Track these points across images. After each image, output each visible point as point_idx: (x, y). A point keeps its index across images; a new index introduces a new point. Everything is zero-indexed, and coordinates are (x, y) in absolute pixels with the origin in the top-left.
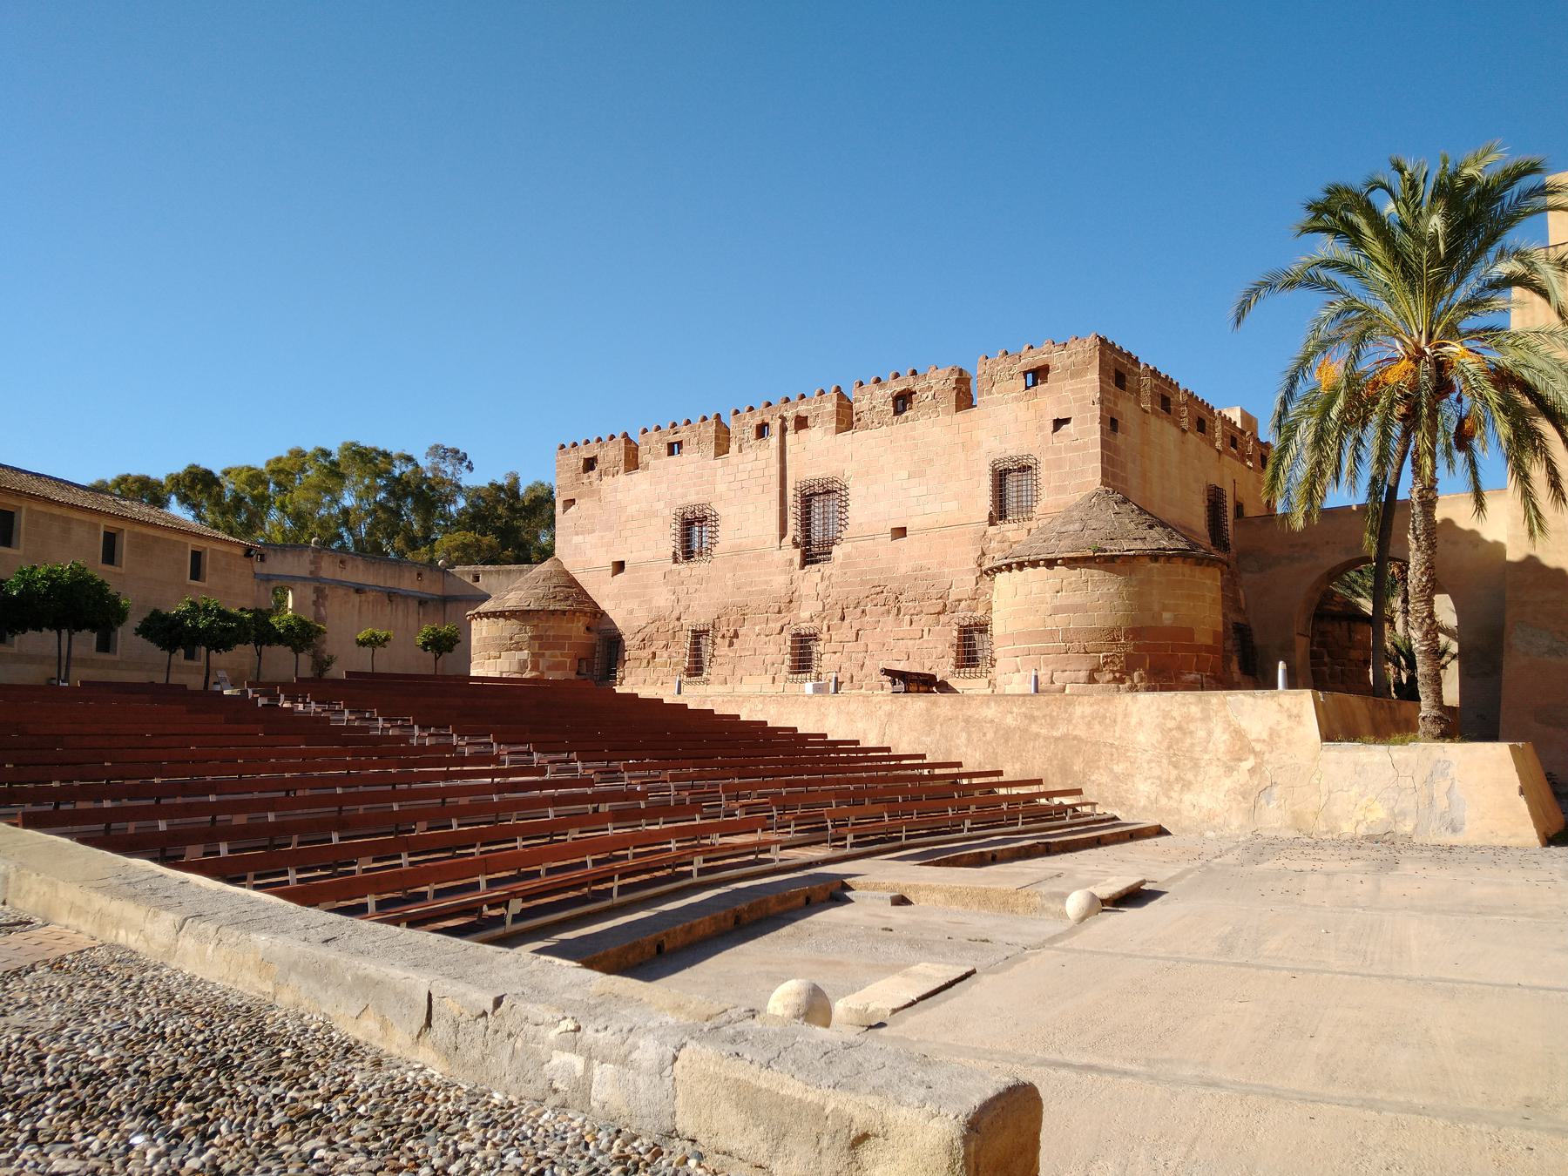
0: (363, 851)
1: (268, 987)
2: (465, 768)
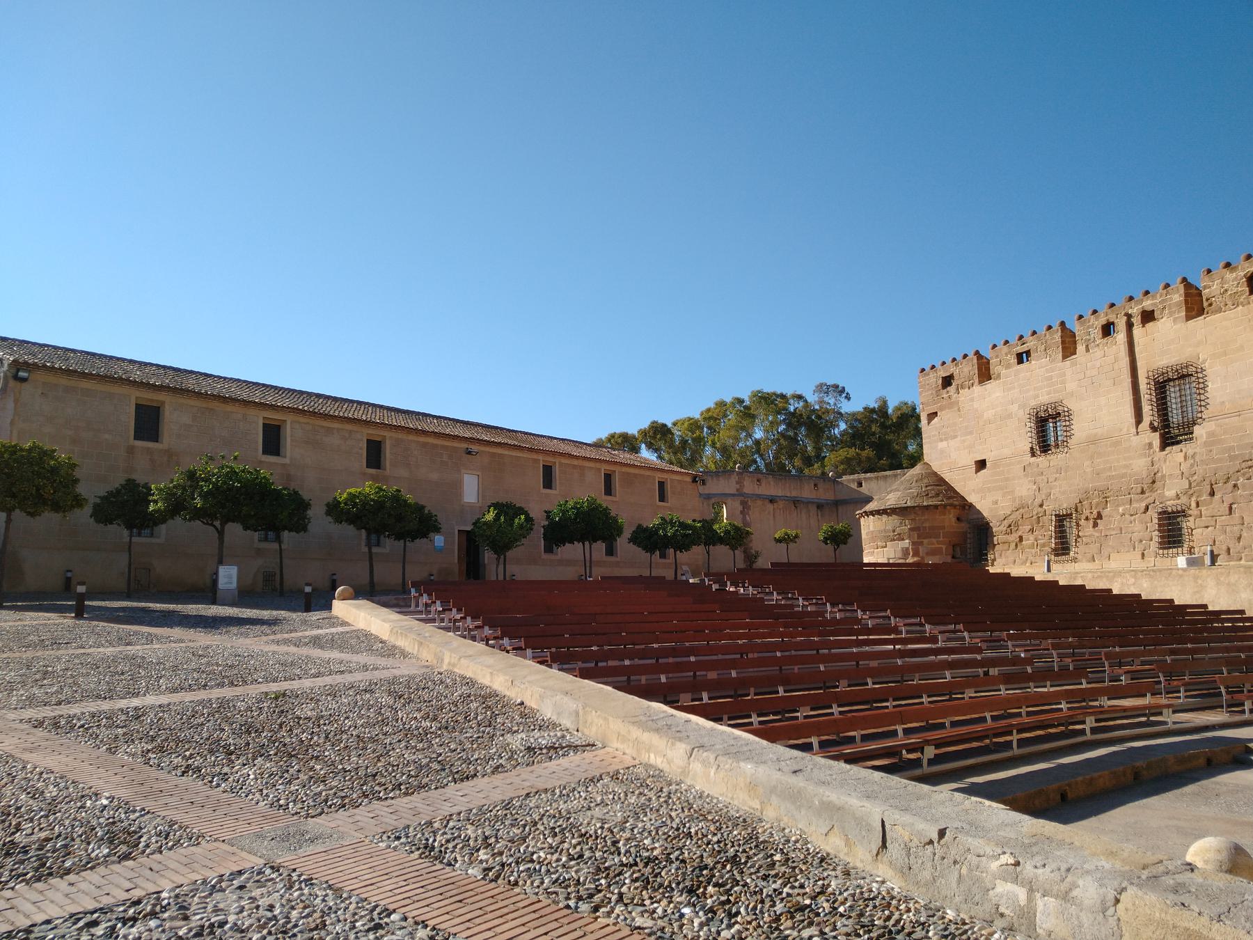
0: (803, 701)
1: (756, 804)
2: (871, 637)
